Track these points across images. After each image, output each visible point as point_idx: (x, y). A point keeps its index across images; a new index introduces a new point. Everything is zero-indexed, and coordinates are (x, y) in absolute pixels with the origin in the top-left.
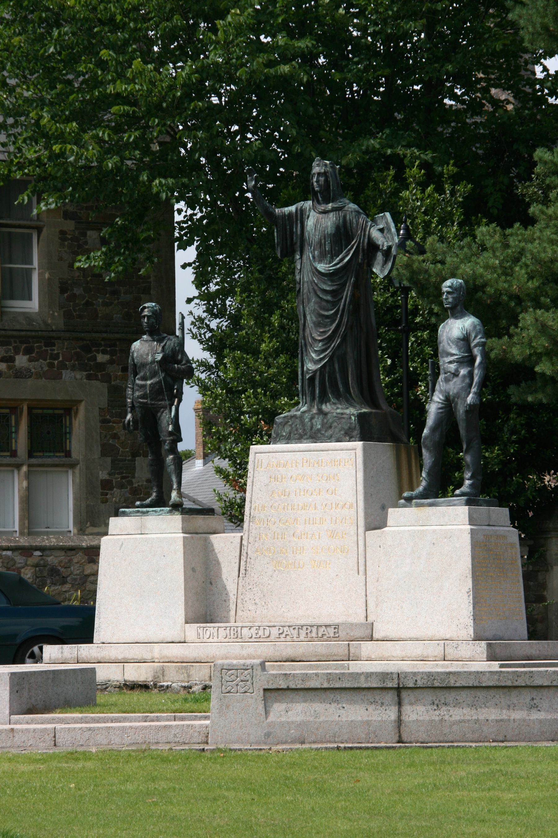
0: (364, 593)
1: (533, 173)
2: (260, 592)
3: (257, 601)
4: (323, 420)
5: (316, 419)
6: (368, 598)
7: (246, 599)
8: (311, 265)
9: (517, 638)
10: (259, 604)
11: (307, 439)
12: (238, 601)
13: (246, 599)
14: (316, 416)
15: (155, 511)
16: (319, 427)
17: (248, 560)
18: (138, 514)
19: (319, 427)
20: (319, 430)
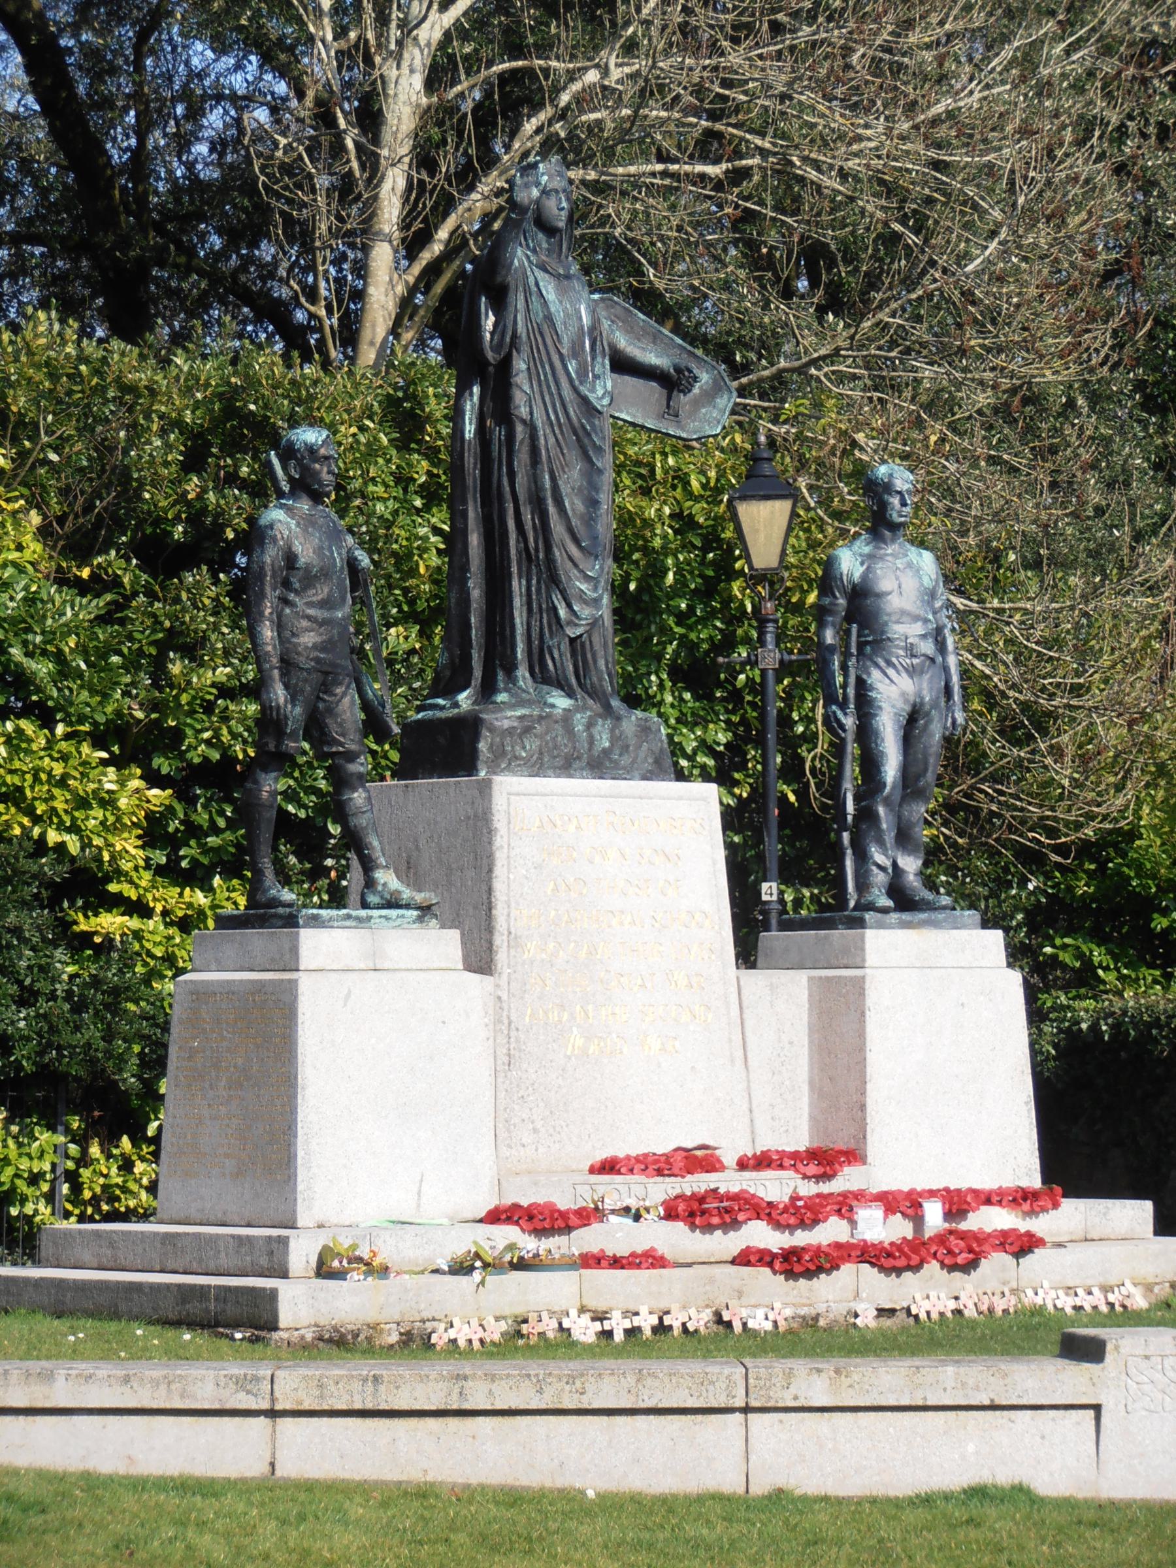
0: (746, 1106)
1: (151, 211)
2: (542, 1104)
3: (539, 1124)
4: (612, 731)
5: (599, 728)
6: (756, 1114)
7: (515, 1120)
8: (575, 390)
9: (198, 1216)
10: (543, 1130)
11: (582, 769)
12: (500, 1125)
13: (515, 1120)
14: (600, 721)
15: (387, 918)
16: (607, 744)
17: (513, 1034)
18: (348, 923)
19: (607, 744)
20: (606, 752)
